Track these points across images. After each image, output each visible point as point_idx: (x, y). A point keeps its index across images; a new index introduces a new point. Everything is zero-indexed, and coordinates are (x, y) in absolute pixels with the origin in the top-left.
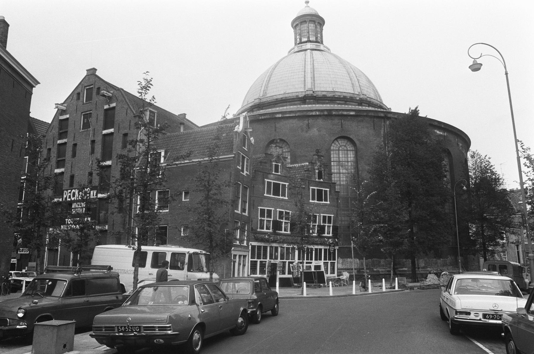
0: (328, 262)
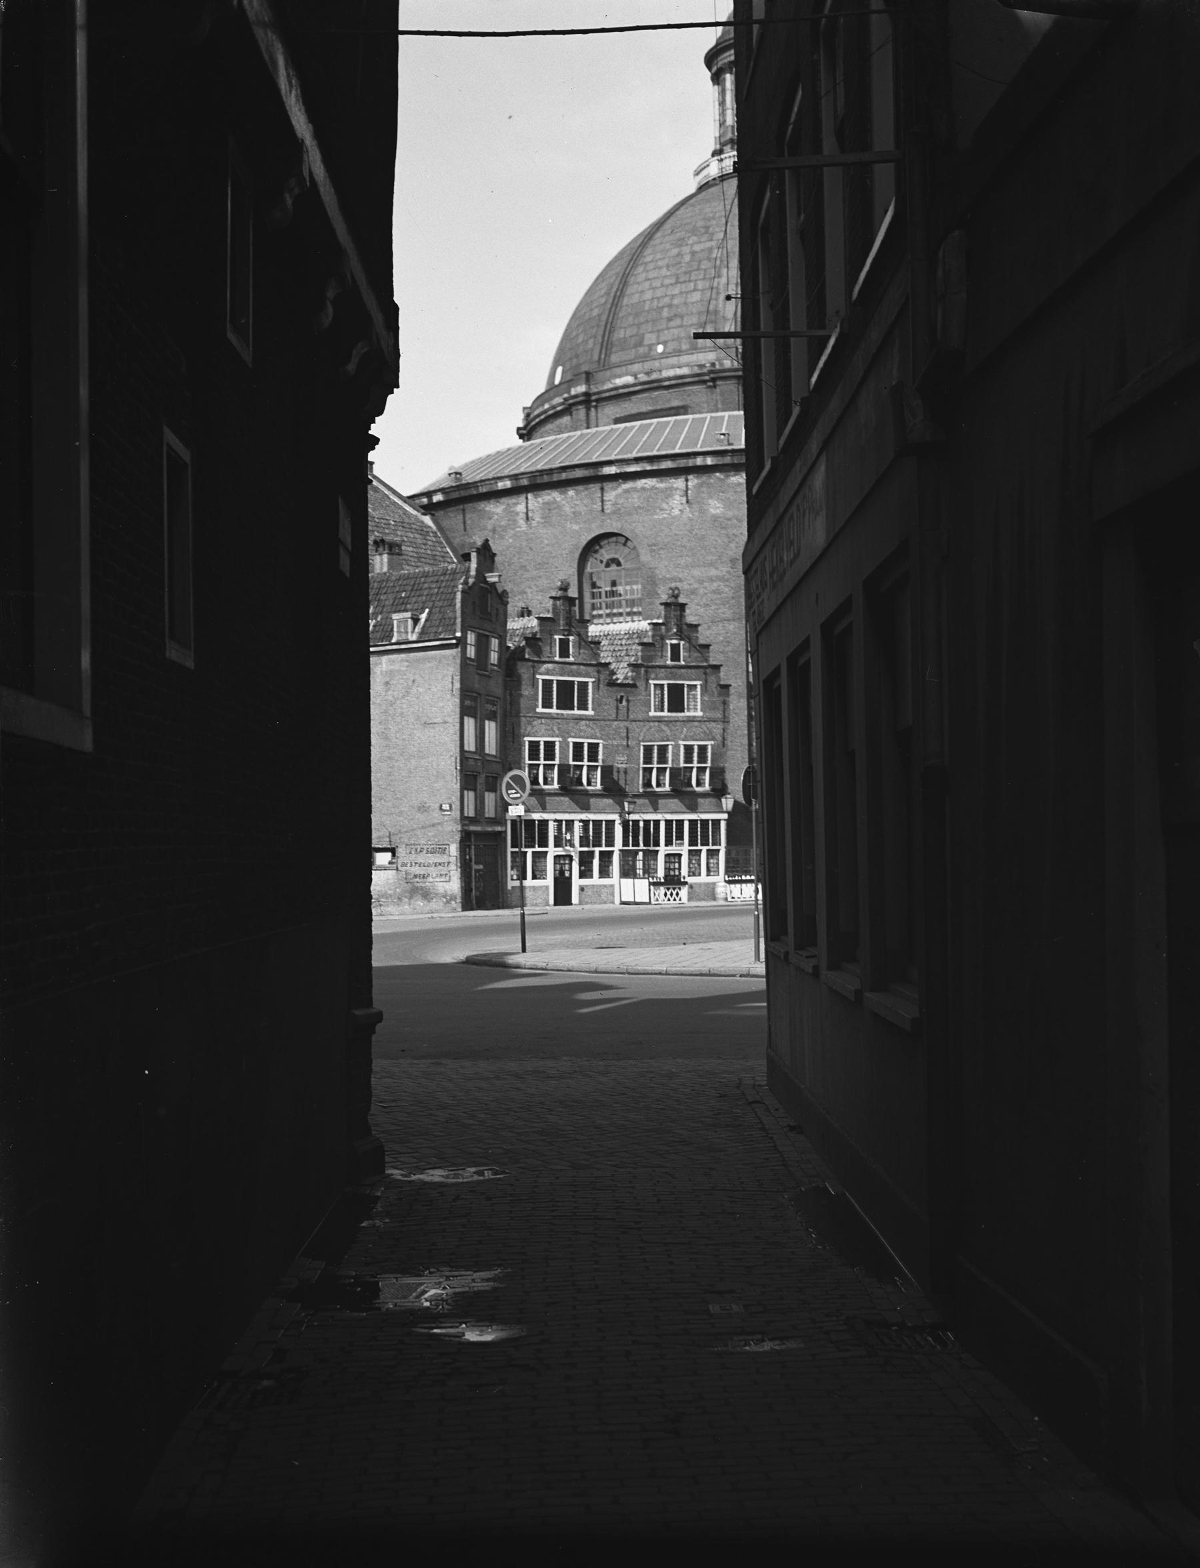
0: (701, 851)
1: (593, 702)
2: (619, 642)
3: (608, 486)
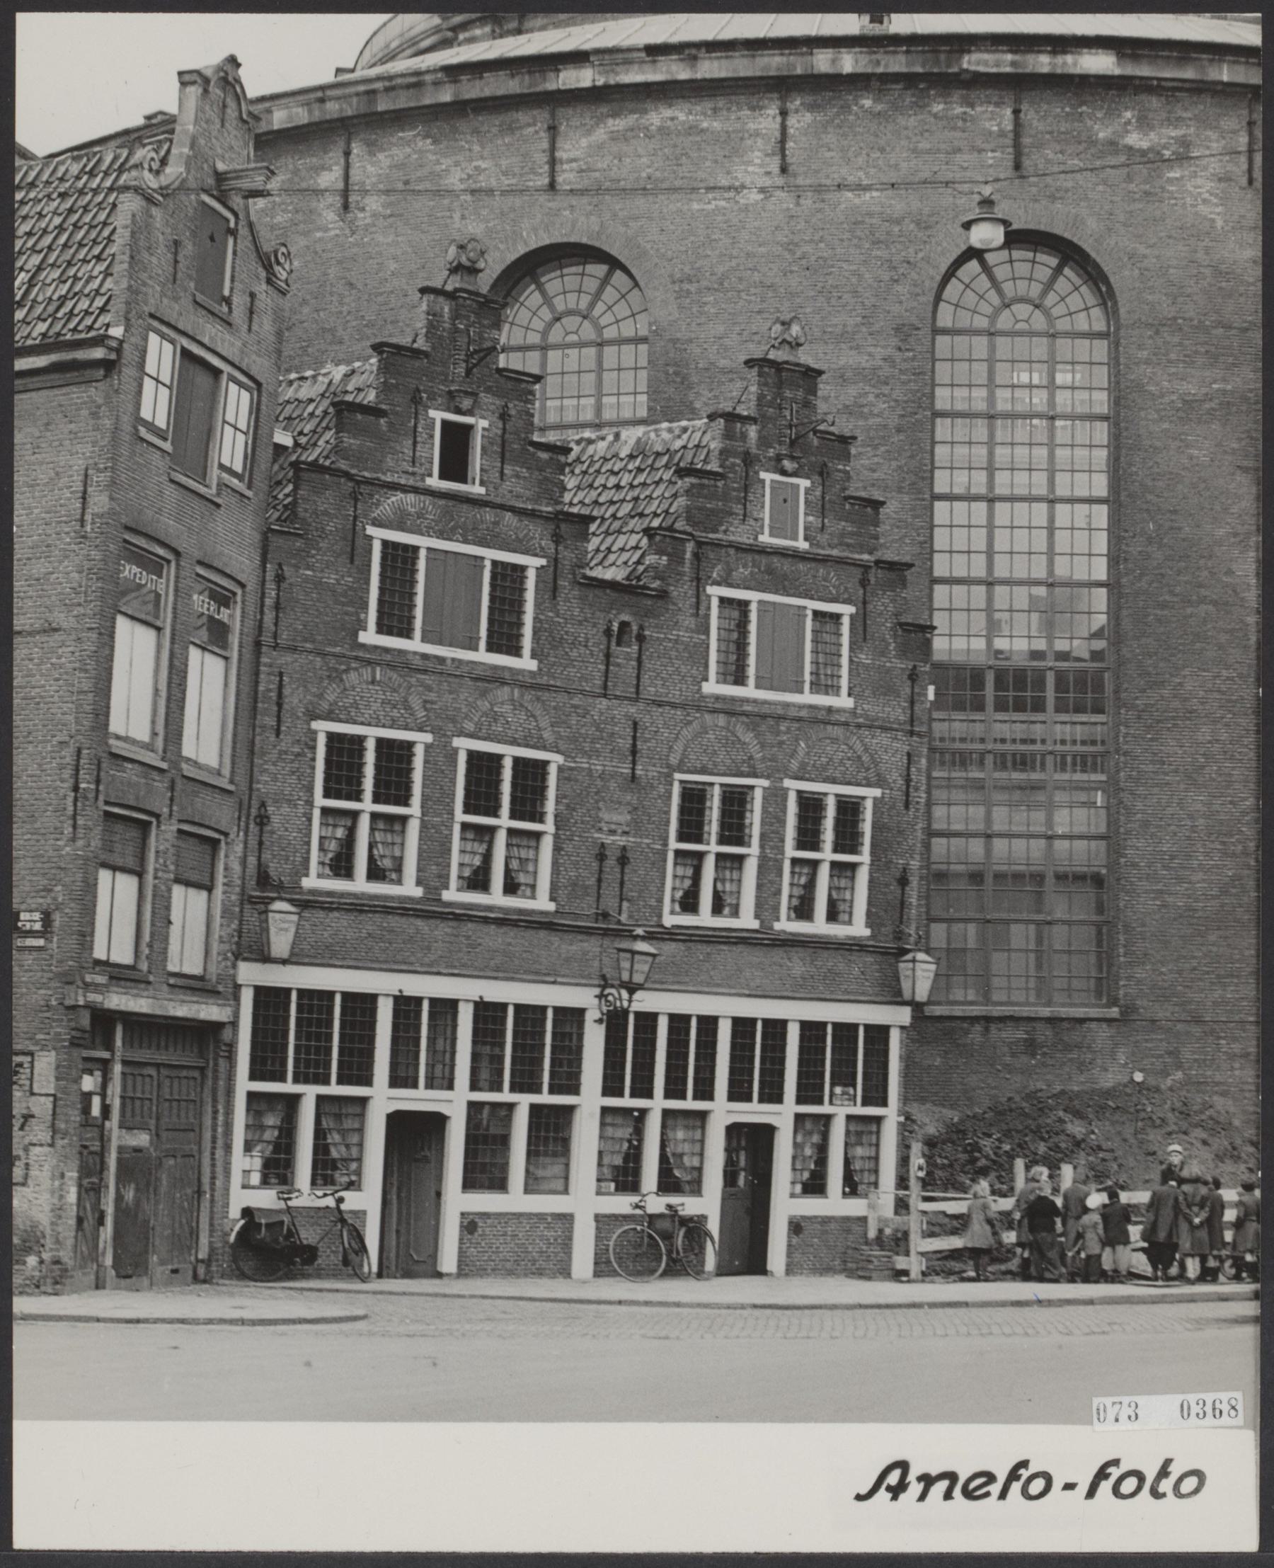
0: (511, 1107)
1: (536, 632)
2: (612, 481)
3: (571, 119)
